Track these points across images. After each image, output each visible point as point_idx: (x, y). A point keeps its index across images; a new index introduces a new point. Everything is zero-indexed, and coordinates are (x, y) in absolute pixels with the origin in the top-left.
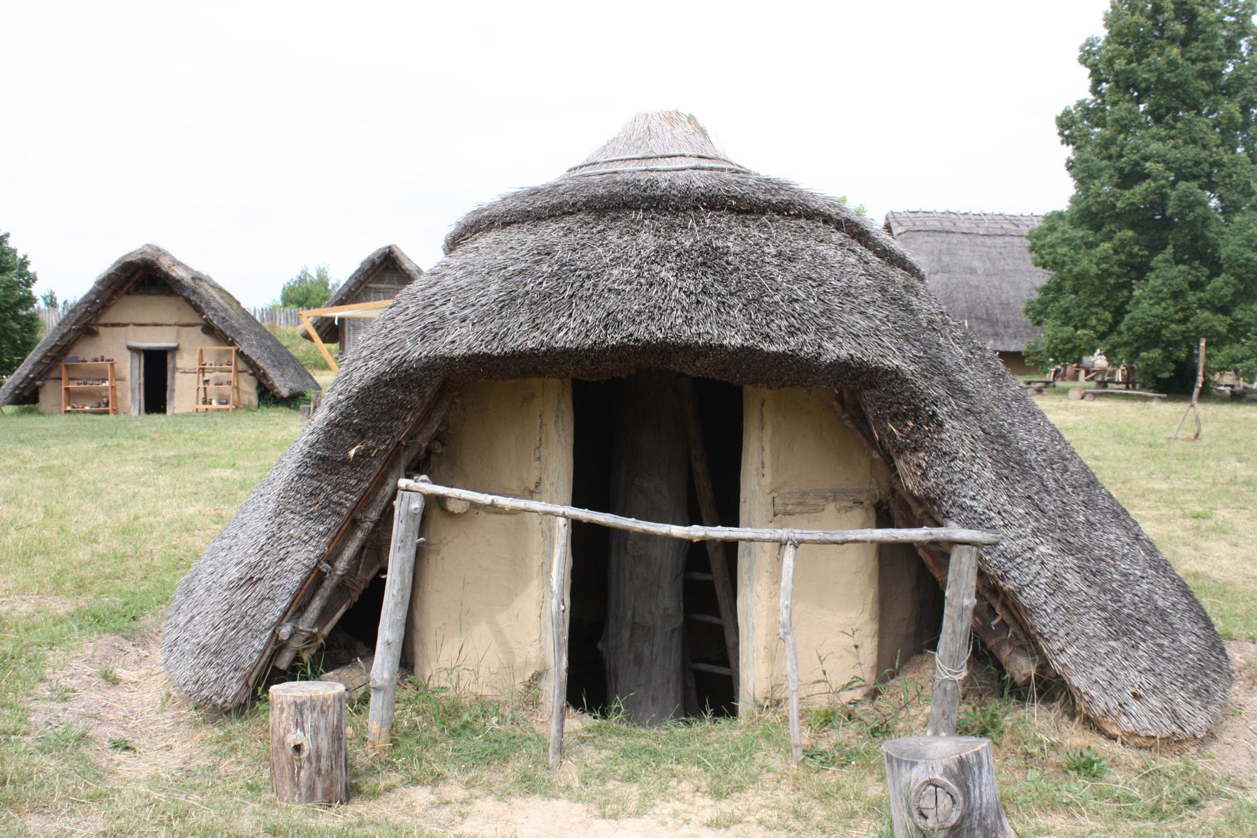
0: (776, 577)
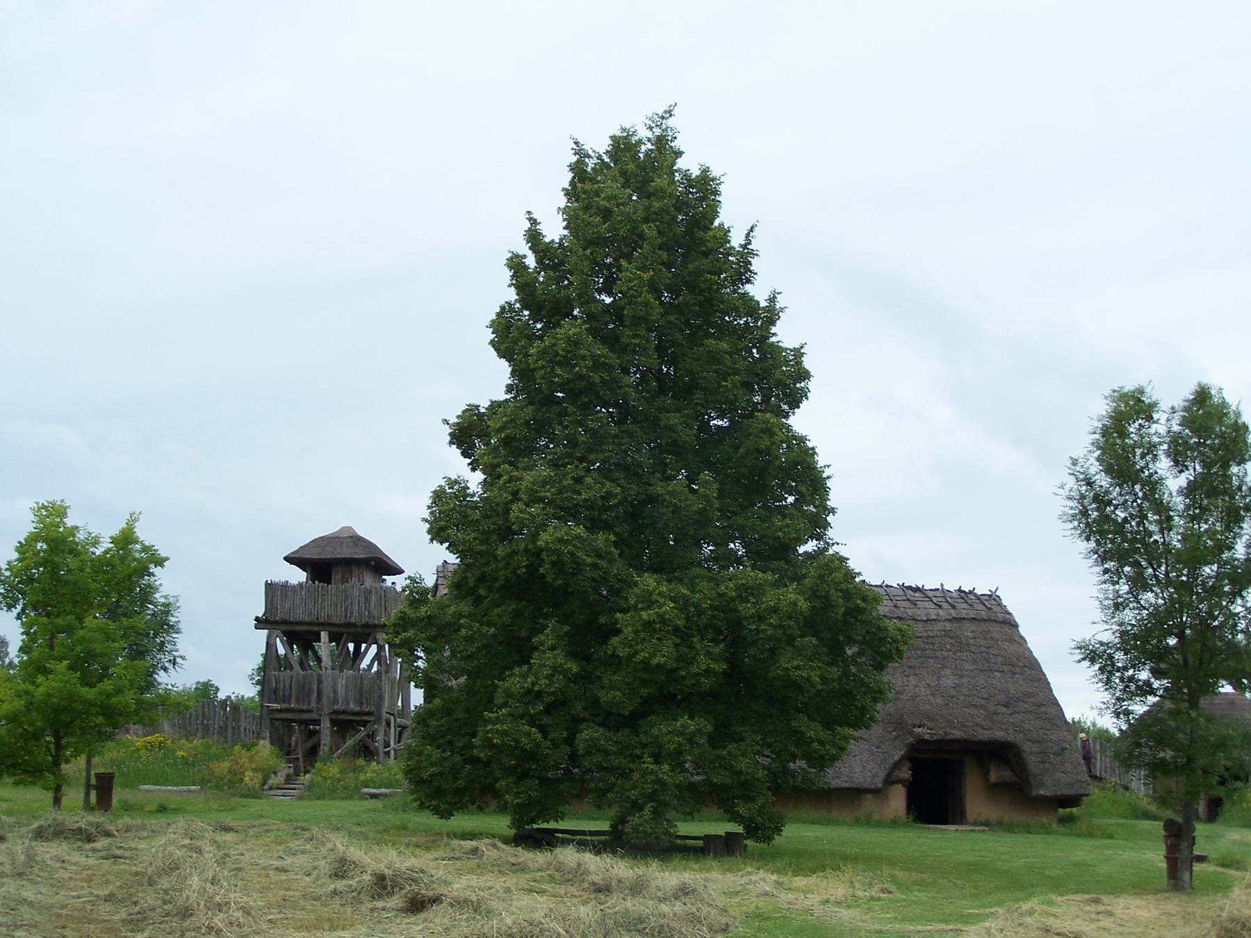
0: (284, 691)
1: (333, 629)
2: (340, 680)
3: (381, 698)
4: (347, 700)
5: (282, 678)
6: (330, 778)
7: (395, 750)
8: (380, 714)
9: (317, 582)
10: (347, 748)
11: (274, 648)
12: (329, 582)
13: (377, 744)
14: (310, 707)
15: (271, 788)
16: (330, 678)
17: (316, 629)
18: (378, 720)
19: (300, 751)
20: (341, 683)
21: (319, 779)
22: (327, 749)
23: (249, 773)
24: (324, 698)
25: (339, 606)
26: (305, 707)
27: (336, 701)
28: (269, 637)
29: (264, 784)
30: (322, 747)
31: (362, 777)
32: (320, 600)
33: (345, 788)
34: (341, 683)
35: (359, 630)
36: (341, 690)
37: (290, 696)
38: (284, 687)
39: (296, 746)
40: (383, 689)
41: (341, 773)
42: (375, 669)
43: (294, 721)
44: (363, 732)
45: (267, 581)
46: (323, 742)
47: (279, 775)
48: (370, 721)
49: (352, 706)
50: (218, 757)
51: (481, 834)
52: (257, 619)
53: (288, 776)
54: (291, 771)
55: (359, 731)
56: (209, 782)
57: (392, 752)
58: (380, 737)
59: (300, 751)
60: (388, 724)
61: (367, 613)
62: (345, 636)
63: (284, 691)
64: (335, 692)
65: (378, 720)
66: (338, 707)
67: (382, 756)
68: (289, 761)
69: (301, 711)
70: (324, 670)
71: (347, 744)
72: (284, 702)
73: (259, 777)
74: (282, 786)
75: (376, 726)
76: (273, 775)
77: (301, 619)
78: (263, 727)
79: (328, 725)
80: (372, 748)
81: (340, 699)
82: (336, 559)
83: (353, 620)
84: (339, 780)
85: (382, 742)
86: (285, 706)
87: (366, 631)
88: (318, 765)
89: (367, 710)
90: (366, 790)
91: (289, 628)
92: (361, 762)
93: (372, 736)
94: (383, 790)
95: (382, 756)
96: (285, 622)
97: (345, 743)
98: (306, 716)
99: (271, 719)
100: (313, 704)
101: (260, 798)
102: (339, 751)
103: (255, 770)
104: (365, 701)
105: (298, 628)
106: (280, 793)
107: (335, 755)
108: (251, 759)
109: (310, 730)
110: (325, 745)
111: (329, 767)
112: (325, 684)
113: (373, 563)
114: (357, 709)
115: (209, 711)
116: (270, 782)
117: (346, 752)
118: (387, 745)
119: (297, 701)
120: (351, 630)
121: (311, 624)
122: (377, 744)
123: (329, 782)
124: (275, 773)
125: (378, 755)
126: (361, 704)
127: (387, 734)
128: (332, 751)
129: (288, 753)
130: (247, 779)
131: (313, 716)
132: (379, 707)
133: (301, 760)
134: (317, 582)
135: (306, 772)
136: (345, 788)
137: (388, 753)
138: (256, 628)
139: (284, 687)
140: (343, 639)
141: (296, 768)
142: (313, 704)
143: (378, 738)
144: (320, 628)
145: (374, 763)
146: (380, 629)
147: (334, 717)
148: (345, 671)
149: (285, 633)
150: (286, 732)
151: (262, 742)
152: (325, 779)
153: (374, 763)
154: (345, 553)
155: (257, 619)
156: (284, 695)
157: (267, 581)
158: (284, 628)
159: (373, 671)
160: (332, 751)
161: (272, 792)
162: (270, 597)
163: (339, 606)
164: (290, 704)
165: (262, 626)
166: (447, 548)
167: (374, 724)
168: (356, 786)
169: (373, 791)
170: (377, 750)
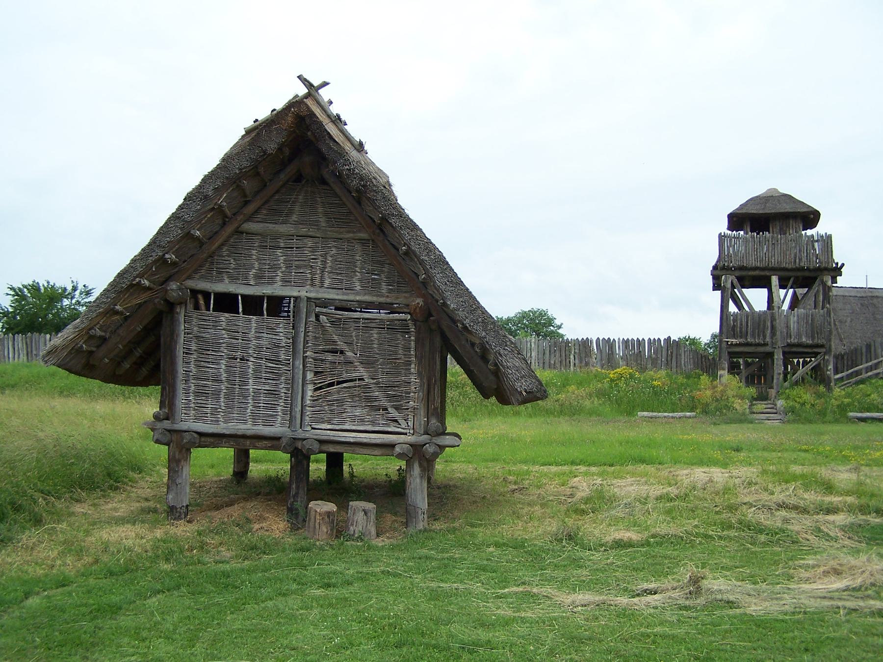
4: (799, 335)
24: (778, 333)
38: (741, 324)
49: (804, 340)
64: (788, 327)
66: (793, 340)
69: (759, 345)
72: (741, 337)
83: (802, 264)
86: (742, 340)
98: (761, 349)
119: (753, 336)
126: (813, 338)
131: (768, 349)
139: (741, 324)
142: (768, 339)
147: (786, 350)
156: (741, 332)
158: (738, 273)
169: (859, 415)
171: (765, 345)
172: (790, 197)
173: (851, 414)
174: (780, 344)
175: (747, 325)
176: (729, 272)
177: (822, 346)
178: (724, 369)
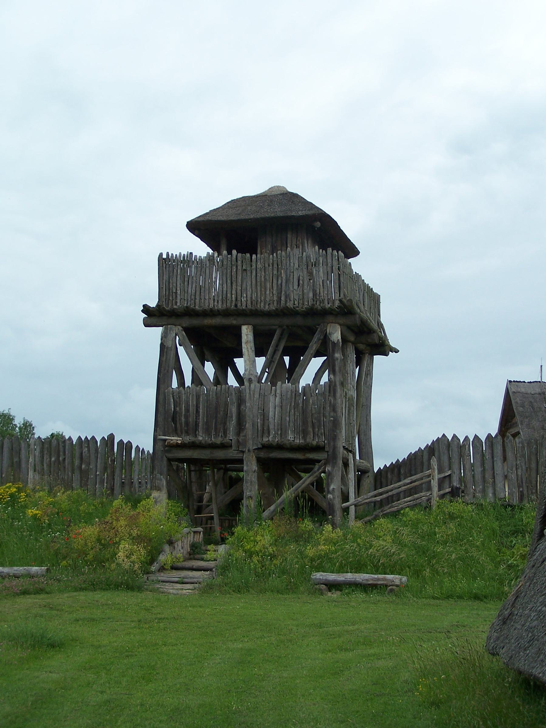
0: (187, 417)
1: (259, 321)
2: (272, 398)
3: (336, 424)
4: (282, 429)
5: (184, 397)
6: (257, 554)
7: (356, 506)
8: (335, 448)
9: (234, 252)
10: (283, 502)
11: (172, 353)
12: (253, 251)
13: (330, 496)
14: (227, 440)
15: (162, 569)
16: (257, 396)
17: (234, 322)
18: (332, 459)
19: (214, 506)
20: (273, 402)
21: (240, 554)
22: (252, 504)
23: (125, 546)
24: (248, 425)
25: (268, 285)
26: (219, 441)
27: (265, 431)
28: (164, 337)
29: (151, 562)
30: (245, 502)
31: (310, 551)
32: (240, 278)
33: (283, 572)
34: (273, 402)
35: (299, 321)
36: (273, 413)
37: (197, 425)
38: (187, 410)
39: (210, 500)
40: (339, 410)
41: (275, 543)
42: (325, 378)
43: (182, 461)
44: (307, 479)
45: (161, 255)
46: (247, 493)
47: (179, 545)
48: (319, 461)
49: (290, 437)
50: (88, 519)
51: (196, 422)
52: (146, 309)
53: (194, 546)
54: (200, 538)
55: (300, 478)
56: (64, 558)
57: (352, 509)
58: (335, 486)
59: (214, 506)
60: (346, 464)
61: (311, 295)
62: (278, 333)
63: (187, 417)
64: (264, 416)
65: (332, 459)
66: (272, 438)
67: (338, 513)
68: (195, 523)
69: (213, 446)
70: (246, 383)
71: (284, 495)
72: (187, 433)
73: (140, 553)
74: (179, 564)
75: (328, 468)
76: (167, 548)
77: (211, 306)
78: (156, 472)
79: (255, 467)
80: (324, 505)
81: (271, 427)
82: (264, 219)
83: (290, 305)
84: (273, 556)
85: (338, 493)
86: (188, 439)
87: (309, 322)
88: (238, 530)
89: (314, 443)
90: (319, 575)
91: (196, 322)
92: (307, 524)
93: (319, 485)
94: (349, 576)
95: (338, 513)
96: (189, 313)
97: (280, 494)
98: (220, 454)
99: (170, 460)
100: (231, 436)
101: (140, 589)
102: (272, 508)
103: (137, 540)
104: (310, 429)
105: (208, 321)
106: (176, 575)
107: (266, 514)
108: (133, 521)
109: (231, 477)
110: (251, 497)
111: (256, 533)
112: (248, 404)
113: (318, 224)
114: (299, 441)
115: (89, 450)
116: (162, 558)
117: (283, 509)
118: (345, 498)
119: (207, 431)
120: (287, 321)
121: (226, 313)
122: (330, 496)
123: (255, 559)
124: (171, 543)
125: (333, 513)
126: (305, 433)
127: (344, 481)
128: (263, 505)
129: (199, 510)
130: (121, 554)
131: (232, 454)
132: (334, 438)
133: (216, 520)
134: (234, 252)
135: (223, 541)
136: (283, 572)
137: (346, 510)
138: (146, 325)
139: (187, 410)
140: (276, 338)
141: (208, 532)
142: (231, 436)
143: (332, 487)
144: (240, 320)
145: (329, 527)
146: (331, 318)
147: (262, 455)
148: (279, 383)
149: (187, 330)
150: (194, 479)
151: (155, 494)
152: (250, 554)
153: (329, 527)
154: (278, 211)
155: (146, 309)
156: (187, 424)
157: (161, 255)
158: (187, 322)
159: (322, 383)
160: (263, 505)
161: (163, 576)
162: (166, 277)
163: (268, 285)
164: (196, 436)
165: (153, 320)
166: (309, 384)
167: (325, 464)
168: (303, 567)
169: (332, 577)
170: (331, 506)
171: (224, 446)
172: (294, 198)
173: (319, 575)
174: (251, 445)
175: (197, 412)
176: (172, 320)
177: (319, 448)
178: (159, 489)
